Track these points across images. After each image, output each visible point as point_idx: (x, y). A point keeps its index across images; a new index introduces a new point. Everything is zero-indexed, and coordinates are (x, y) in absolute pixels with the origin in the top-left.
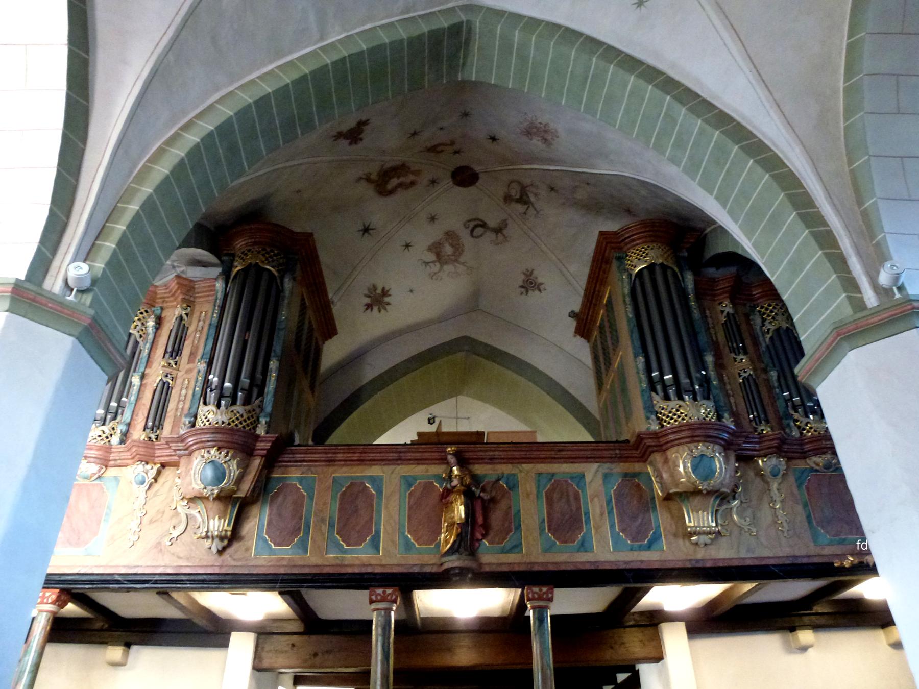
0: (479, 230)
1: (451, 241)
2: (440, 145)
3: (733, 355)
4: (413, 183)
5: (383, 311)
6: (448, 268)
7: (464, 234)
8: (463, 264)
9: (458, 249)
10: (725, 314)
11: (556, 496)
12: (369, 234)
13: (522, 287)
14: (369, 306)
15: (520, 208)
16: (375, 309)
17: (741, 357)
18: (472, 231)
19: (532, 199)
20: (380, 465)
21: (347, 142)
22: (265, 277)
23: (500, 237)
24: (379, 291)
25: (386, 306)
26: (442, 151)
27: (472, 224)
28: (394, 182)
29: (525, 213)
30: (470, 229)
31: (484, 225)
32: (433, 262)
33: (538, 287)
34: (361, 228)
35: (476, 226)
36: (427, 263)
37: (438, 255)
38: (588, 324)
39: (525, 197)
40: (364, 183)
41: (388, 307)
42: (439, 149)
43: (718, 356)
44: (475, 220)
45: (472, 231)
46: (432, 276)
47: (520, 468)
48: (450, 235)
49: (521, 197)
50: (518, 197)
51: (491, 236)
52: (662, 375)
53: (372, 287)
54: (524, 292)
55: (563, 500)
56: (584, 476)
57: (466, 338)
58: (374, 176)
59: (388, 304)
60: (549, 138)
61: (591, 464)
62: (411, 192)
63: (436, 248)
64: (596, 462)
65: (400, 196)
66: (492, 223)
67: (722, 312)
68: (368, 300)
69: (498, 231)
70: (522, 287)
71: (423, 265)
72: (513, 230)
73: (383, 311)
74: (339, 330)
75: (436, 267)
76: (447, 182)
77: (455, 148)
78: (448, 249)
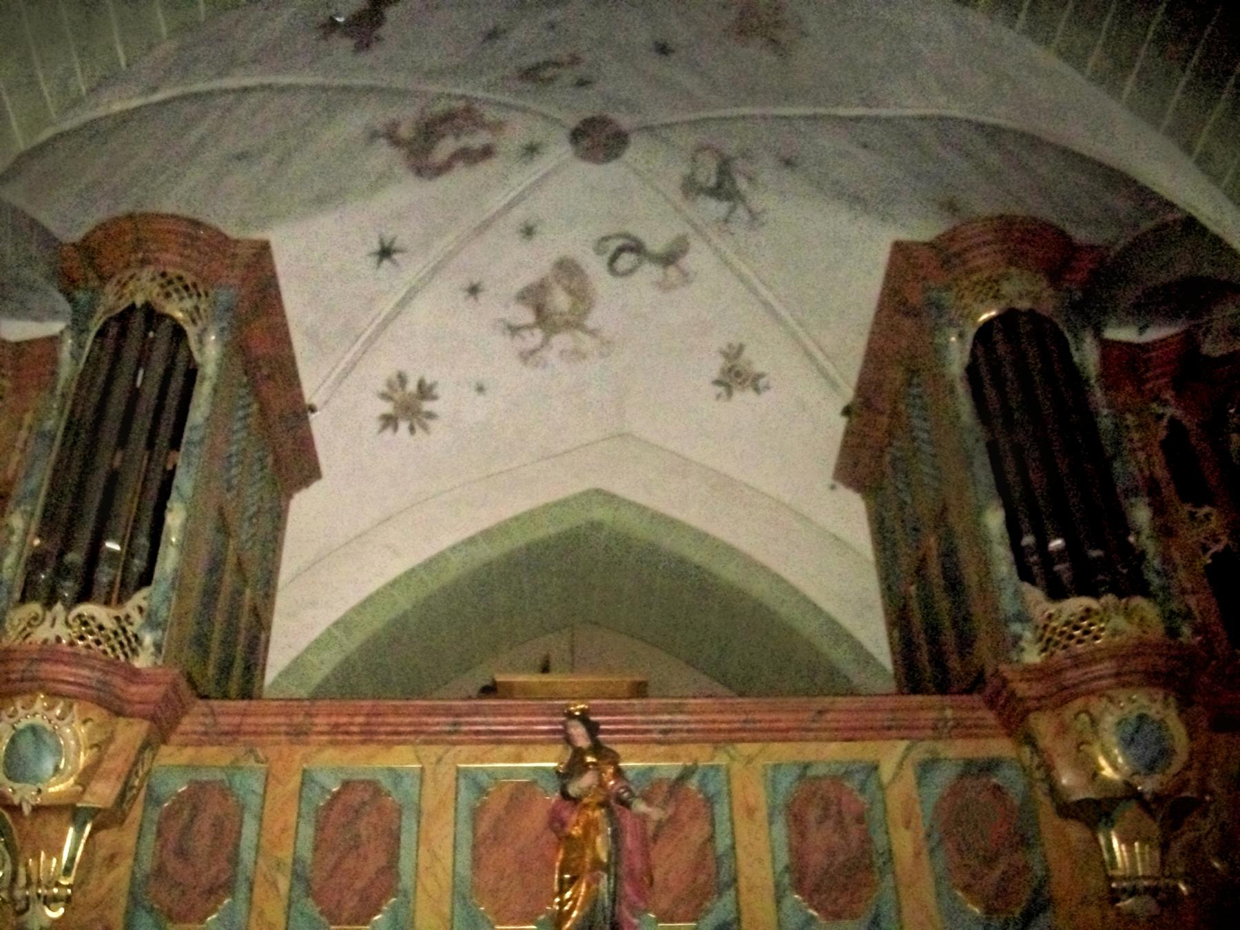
0: (626, 260)
1: (566, 282)
2: (547, 64)
3: (1188, 507)
4: (487, 152)
5: (419, 431)
6: (562, 340)
7: (595, 267)
8: (593, 333)
9: (582, 296)
10: (1165, 422)
11: (813, 814)
12: (394, 262)
13: (718, 383)
14: (389, 421)
15: (716, 208)
16: (404, 426)
17: (1206, 509)
18: (613, 259)
19: (742, 184)
20: (412, 743)
21: (349, 43)
22: (165, 330)
23: (672, 271)
24: (412, 387)
25: (425, 420)
26: (551, 80)
27: (614, 245)
28: (446, 147)
29: (726, 221)
30: (609, 255)
31: (636, 247)
32: (528, 327)
33: (755, 382)
34: (376, 247)
35: (621, 250)
36: (514, 330)
37: (539, 310)
38: (803, 725)
39: (727, 185)
40: (383, 146)
41: (431, 424)
42: (548, 73)
43: (1159, 509)
44: (618, 236)
45: (613, 259)
46: (527, 356)
47: (732, 752)
48: (567, 269)
49: (719, 185)
50: (713, 181)
51: (651, 271)
52: (1042, 543)
53: (395, 378)
54: (724, 394)
55: (830, 823)
56: (875, 768)
57: (598, 491)
58: (405, 132)
59: (431, 415)
60: (783, 36)
61: (888, 744)
62: (486, 169)
63: (535, 297)
64: (902, 739)
65: (461, 179)
66: (657, 242)
67: (1160, 417)
68: (387, 408)
69: (669, 259)
70: (718, 383)
71: (509, 332)
72: (698, 259)
73: (419, 431)
74: (324, 468)
75: (538, 336)
76: (559, 151)
77: (582, 71)
78: (560, 300)
